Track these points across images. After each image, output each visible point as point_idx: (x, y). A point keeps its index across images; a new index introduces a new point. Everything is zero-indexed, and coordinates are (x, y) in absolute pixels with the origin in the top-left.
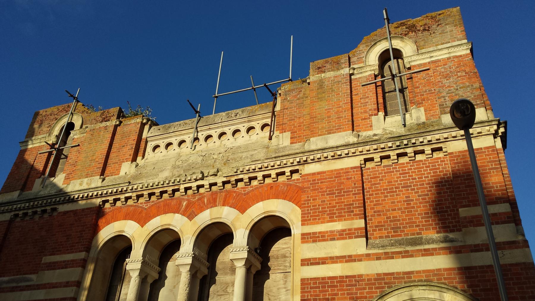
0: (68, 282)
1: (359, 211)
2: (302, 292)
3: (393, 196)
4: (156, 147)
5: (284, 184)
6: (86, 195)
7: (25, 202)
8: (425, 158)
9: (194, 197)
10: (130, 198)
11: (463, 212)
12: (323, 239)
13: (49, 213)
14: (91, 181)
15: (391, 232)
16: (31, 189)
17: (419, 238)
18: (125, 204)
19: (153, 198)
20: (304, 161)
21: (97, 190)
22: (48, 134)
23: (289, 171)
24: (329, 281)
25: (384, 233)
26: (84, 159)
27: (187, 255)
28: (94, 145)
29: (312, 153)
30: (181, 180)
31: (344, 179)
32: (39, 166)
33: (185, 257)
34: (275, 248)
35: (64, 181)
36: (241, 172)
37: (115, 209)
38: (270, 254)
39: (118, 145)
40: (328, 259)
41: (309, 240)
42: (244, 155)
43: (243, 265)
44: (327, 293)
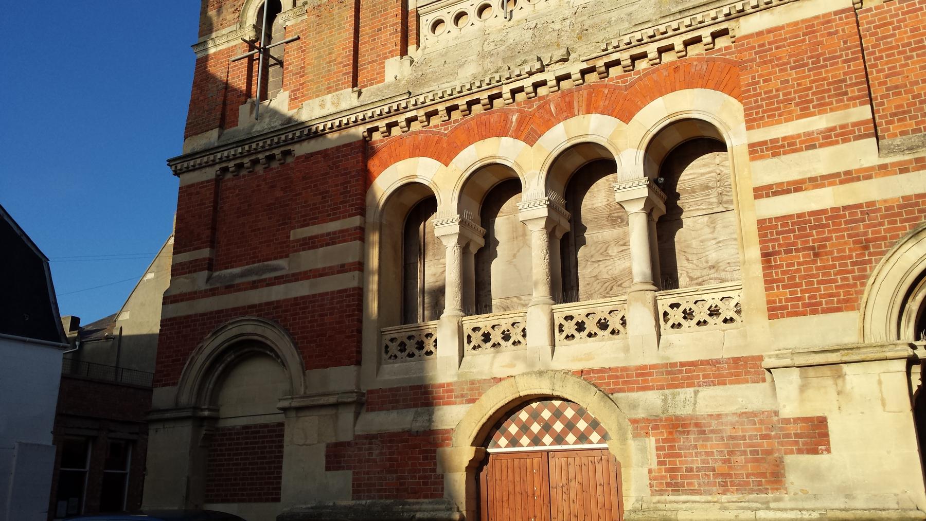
0: (343, 266)
1: (357, 199)
2: (761, 242)
4: (438, 23)
5: (700, 59)
6: (337, 123)
7: (235, 145)
9: (529, 105)
10: (415, 119)
12: (792, 149)
13: (279, 160)
14: (339, 99)
16: (235, 123)
18: (406, 132)
19: (456, 115)
20: (739, 12)
22: (238, 26)
25: (910, 125)
26: (316, 61)
28: (326, 34)
30: (503, 76)
32: (239, 82)
34: (686, 175)
35: (290, 104)
36: (518, 77)
37: (392, 141)
38: (678, 187)
39: (370, 29)
41: (765, 153)
42: (614, 16)
43: (642, 209)
44: (810, 238)
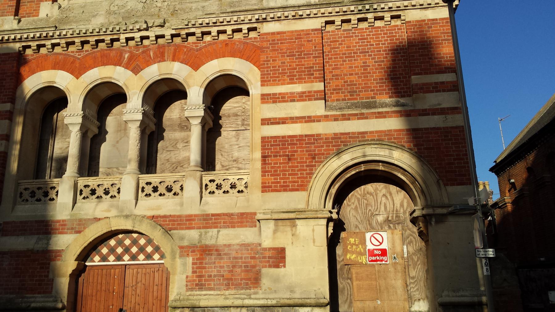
2: (262, 149)
3: (351, 60)
5: (240, 41)
8: (383, 25)
10: (58, 44)
11: (415, 79)
12: (283, 100)
14: (3, 22)
15: (347, 96)
17: (373, 101)
18: (51, 52)
19: (87, 47)
20: (264, 19)
21: (14, 33)
23: (247, 28)
24: (289, 139)
25: (341, 96)
27: (137, 111)
29: (272, 11)
30: (122, 28)
31: (304, 41)
33: (130, 113)
34: (226, 106)
37: (40, 57)
38: (221, 112)
40: (288, 119)
43: (200, 123)
